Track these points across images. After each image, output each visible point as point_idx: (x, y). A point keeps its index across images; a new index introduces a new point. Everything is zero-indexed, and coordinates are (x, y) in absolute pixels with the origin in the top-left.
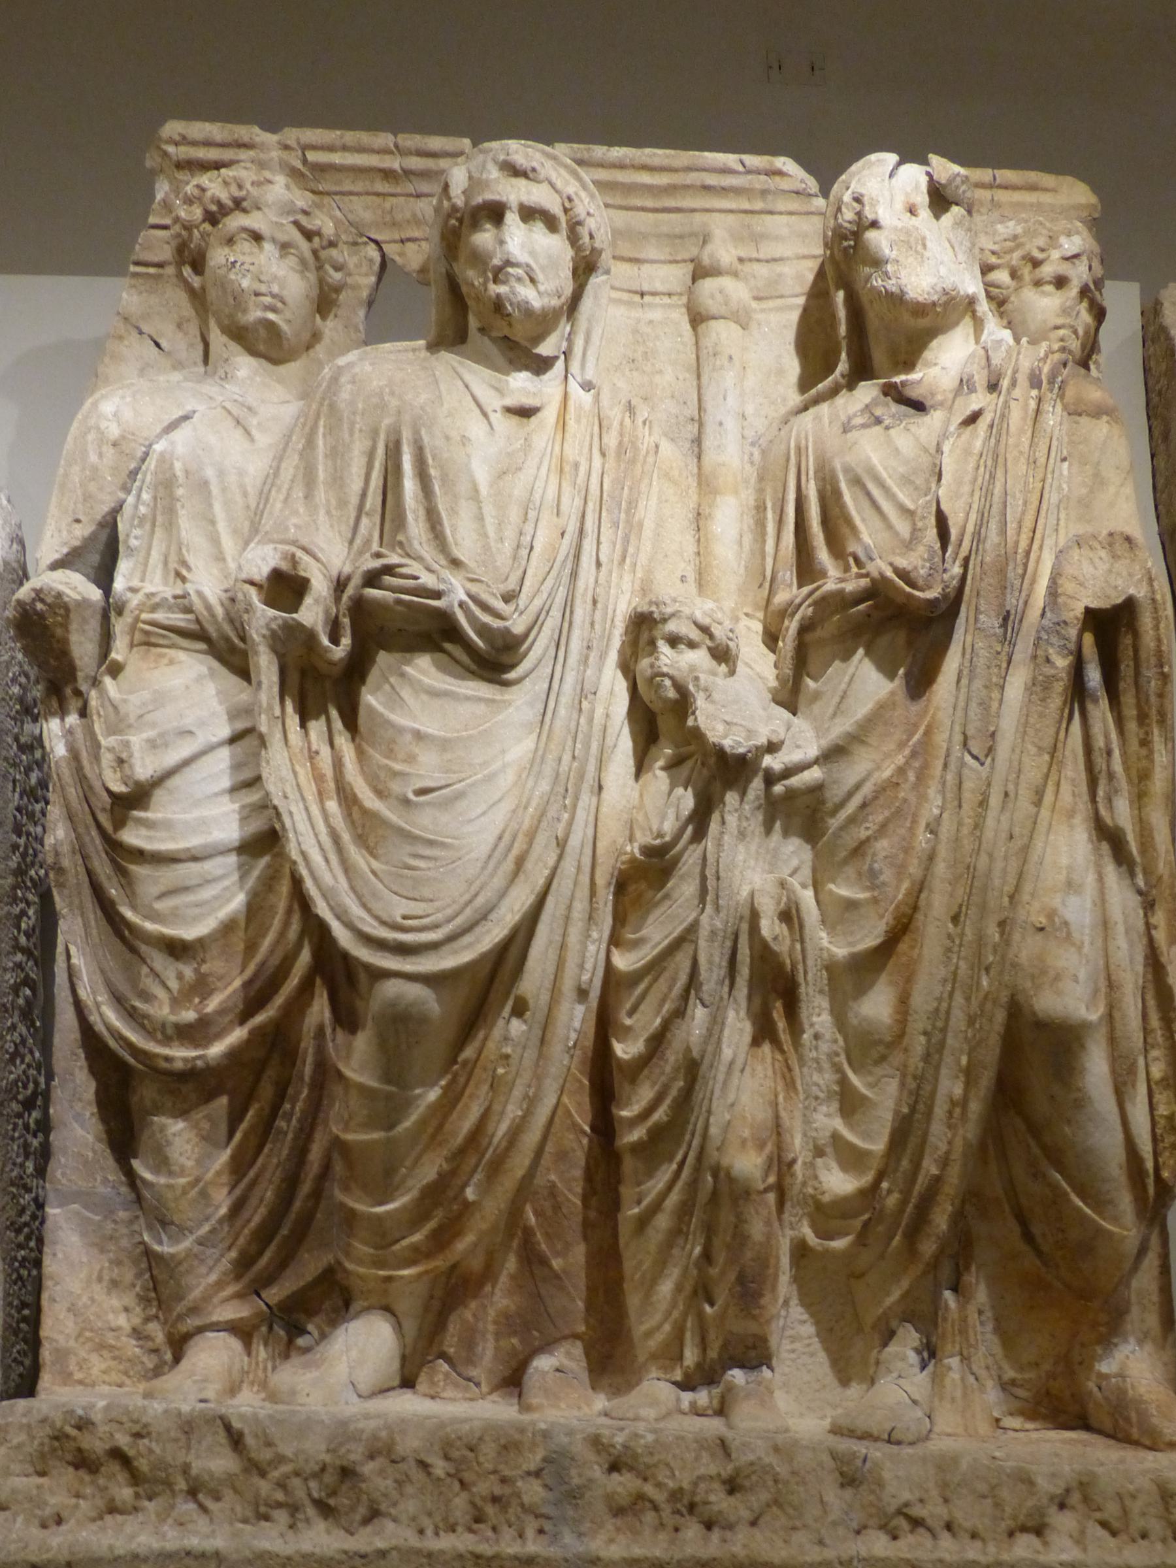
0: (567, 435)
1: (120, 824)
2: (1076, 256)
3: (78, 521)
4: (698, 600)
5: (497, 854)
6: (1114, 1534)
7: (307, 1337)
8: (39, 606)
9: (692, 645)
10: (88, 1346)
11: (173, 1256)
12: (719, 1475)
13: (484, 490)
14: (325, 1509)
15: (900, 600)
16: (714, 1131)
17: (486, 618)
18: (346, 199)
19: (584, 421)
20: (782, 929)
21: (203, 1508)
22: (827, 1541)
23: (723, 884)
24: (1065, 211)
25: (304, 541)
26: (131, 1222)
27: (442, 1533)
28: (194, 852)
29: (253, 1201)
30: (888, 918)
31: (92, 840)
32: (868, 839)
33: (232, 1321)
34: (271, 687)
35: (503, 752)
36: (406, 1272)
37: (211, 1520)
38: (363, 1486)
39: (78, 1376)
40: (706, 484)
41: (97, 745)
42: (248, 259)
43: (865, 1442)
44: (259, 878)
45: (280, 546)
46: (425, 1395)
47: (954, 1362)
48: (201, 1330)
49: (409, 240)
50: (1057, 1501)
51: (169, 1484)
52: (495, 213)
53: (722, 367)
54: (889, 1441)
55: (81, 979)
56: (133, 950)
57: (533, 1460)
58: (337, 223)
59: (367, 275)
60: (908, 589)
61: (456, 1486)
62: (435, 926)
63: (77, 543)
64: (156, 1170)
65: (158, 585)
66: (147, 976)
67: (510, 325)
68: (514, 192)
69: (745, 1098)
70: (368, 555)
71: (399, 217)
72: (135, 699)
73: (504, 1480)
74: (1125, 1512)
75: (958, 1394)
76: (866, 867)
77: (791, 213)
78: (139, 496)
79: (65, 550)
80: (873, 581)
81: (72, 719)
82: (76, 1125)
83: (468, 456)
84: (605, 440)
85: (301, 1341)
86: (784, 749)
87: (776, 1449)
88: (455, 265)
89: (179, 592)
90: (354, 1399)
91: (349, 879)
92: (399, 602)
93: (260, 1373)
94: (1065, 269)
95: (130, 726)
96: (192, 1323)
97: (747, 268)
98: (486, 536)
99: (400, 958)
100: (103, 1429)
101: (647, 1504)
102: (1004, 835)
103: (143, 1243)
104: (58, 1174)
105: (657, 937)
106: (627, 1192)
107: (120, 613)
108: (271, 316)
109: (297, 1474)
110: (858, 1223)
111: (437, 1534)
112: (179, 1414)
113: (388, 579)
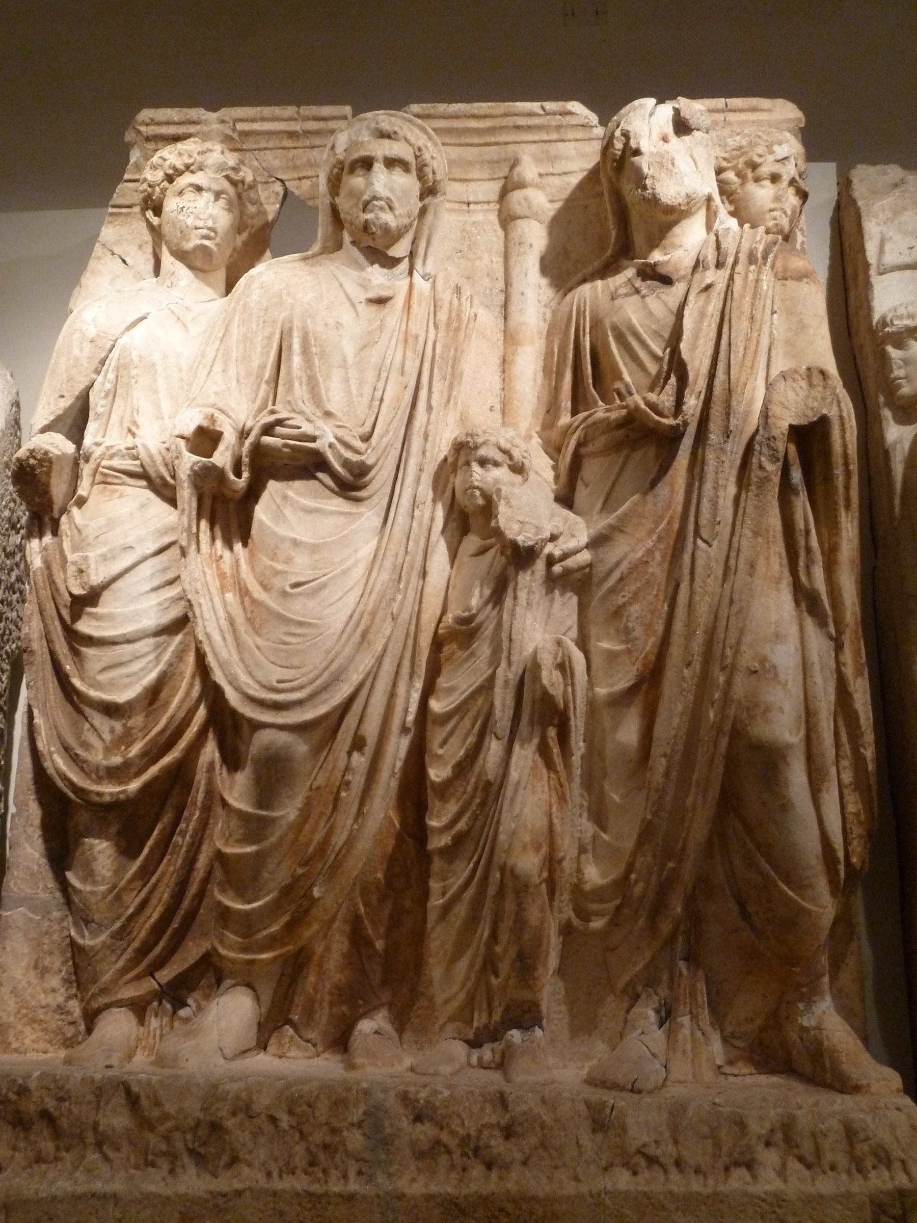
0: (412, 316)
1: (76, 615)
2: (786, 158)
3: (62, 397)
4: (502, 431)
5: (348, 629)
6: (809, 1167)
7: (188, 1008)
8: (32, 461)
9: (496, 464)
10: (25, 1020)
11: (92, 947)
12: (499, 1123)
13: (350, 361)
14: (200, 1159)
15: (651, 425)
16: (502, 837)
17: (349, 455)
18: (262, 153)
19: (423, 304)
20: (557, 675)
21: (106, 1158)
22: (581, 1177)
23: (516, 645)
24: (777, 126)
25: (220, 405)
26: (62, 920)
27: (284, 1176)
28: (128, 636)
29: (154, 901)
30: (639, 664)
31: (56, 628)
32: (624, 605)
33: (132, 998)
34: (190, 512)
35: (356, 551)
36: (265, 956)
37: (112, 1168)
38: (227, 1137)
39: (15, 1045)
40: (510, 338)
41: (64, 560)
42: (192, 205)
43: (613, 1093)
44: (173, 652)
45: (202, 409)
46: (274, 1055)
47: (686, 1020)
48: (108, 1006)
49: (304, 178)
50: (763, 1140)
51: (81, 1138)
52: (367, 164)
53: (525, 252)
54: (632, 1091)
55: (40, 734)
56: (80, 711)
57: (357, 1114)
58: (255, 170)
59: (273, 204)
60: (657, 418)
61: (297, 1136)
62: (302, 687)
63: (60, 412)
64: (84, 880)
65: (116, 439)
66: (88, 730)
67: (374, 239)
68: (382, 149)
69: (527, 811)
70: (265, 412)
71: (298, 163)
72: (93, 524)
73: (334, 1131)
74: (817, 1148)
75: (689, 1047)
76: (622, 626)
77: (577, 140)
78: (106, 376)
79: (52, 418)
80: (629, 413)
81: (48, 539)
82: (27, 845)
83: (340, 336)
84: (438, 317)
85: (183, 1013)
86: (561, 539)
87: (543, 1101)
88: (336, 199)
89: (130, 445)
90: (221, 1061)
91: (240, 653)
92: (286, 445)
93: (151, 1040)
94: (777, 168)
95: (89, 544)
96: (103, 1000)
97: (545, 180)
98: (349, 392)
99: (274, 713)
100: (36, 1095)
101: (442, 1149)
102: (726, 601)
103: (70, 936)
104: (12, 884)
105: (464, 686)
106: (435, 885)
107: (87, 460)
108: (207, 242)
109: (177, 1128)
110: (611, 906)
111: (280, 1176)
112: (93, 1081)
113: (279, 429)
